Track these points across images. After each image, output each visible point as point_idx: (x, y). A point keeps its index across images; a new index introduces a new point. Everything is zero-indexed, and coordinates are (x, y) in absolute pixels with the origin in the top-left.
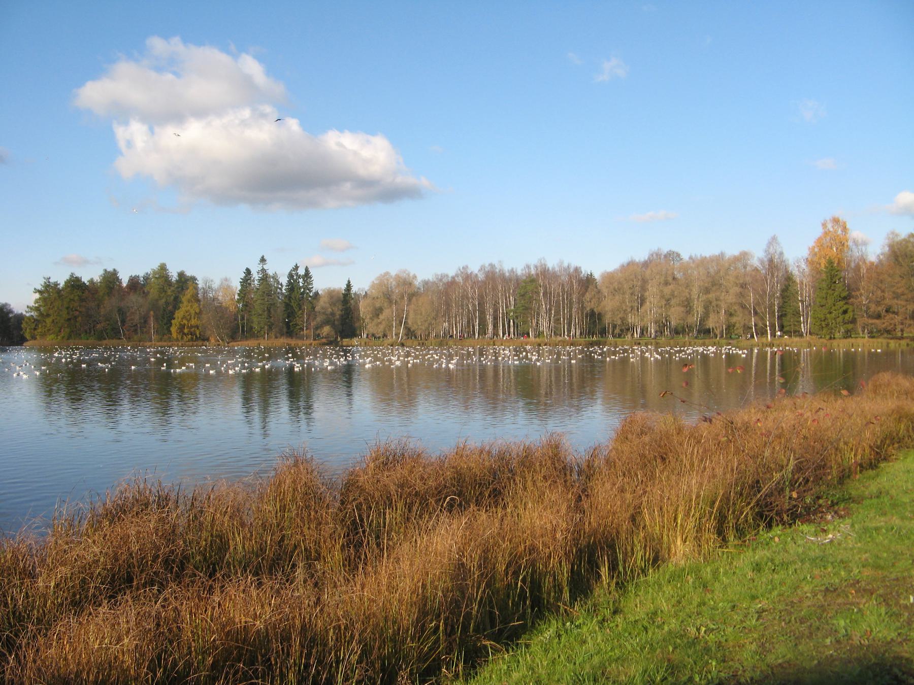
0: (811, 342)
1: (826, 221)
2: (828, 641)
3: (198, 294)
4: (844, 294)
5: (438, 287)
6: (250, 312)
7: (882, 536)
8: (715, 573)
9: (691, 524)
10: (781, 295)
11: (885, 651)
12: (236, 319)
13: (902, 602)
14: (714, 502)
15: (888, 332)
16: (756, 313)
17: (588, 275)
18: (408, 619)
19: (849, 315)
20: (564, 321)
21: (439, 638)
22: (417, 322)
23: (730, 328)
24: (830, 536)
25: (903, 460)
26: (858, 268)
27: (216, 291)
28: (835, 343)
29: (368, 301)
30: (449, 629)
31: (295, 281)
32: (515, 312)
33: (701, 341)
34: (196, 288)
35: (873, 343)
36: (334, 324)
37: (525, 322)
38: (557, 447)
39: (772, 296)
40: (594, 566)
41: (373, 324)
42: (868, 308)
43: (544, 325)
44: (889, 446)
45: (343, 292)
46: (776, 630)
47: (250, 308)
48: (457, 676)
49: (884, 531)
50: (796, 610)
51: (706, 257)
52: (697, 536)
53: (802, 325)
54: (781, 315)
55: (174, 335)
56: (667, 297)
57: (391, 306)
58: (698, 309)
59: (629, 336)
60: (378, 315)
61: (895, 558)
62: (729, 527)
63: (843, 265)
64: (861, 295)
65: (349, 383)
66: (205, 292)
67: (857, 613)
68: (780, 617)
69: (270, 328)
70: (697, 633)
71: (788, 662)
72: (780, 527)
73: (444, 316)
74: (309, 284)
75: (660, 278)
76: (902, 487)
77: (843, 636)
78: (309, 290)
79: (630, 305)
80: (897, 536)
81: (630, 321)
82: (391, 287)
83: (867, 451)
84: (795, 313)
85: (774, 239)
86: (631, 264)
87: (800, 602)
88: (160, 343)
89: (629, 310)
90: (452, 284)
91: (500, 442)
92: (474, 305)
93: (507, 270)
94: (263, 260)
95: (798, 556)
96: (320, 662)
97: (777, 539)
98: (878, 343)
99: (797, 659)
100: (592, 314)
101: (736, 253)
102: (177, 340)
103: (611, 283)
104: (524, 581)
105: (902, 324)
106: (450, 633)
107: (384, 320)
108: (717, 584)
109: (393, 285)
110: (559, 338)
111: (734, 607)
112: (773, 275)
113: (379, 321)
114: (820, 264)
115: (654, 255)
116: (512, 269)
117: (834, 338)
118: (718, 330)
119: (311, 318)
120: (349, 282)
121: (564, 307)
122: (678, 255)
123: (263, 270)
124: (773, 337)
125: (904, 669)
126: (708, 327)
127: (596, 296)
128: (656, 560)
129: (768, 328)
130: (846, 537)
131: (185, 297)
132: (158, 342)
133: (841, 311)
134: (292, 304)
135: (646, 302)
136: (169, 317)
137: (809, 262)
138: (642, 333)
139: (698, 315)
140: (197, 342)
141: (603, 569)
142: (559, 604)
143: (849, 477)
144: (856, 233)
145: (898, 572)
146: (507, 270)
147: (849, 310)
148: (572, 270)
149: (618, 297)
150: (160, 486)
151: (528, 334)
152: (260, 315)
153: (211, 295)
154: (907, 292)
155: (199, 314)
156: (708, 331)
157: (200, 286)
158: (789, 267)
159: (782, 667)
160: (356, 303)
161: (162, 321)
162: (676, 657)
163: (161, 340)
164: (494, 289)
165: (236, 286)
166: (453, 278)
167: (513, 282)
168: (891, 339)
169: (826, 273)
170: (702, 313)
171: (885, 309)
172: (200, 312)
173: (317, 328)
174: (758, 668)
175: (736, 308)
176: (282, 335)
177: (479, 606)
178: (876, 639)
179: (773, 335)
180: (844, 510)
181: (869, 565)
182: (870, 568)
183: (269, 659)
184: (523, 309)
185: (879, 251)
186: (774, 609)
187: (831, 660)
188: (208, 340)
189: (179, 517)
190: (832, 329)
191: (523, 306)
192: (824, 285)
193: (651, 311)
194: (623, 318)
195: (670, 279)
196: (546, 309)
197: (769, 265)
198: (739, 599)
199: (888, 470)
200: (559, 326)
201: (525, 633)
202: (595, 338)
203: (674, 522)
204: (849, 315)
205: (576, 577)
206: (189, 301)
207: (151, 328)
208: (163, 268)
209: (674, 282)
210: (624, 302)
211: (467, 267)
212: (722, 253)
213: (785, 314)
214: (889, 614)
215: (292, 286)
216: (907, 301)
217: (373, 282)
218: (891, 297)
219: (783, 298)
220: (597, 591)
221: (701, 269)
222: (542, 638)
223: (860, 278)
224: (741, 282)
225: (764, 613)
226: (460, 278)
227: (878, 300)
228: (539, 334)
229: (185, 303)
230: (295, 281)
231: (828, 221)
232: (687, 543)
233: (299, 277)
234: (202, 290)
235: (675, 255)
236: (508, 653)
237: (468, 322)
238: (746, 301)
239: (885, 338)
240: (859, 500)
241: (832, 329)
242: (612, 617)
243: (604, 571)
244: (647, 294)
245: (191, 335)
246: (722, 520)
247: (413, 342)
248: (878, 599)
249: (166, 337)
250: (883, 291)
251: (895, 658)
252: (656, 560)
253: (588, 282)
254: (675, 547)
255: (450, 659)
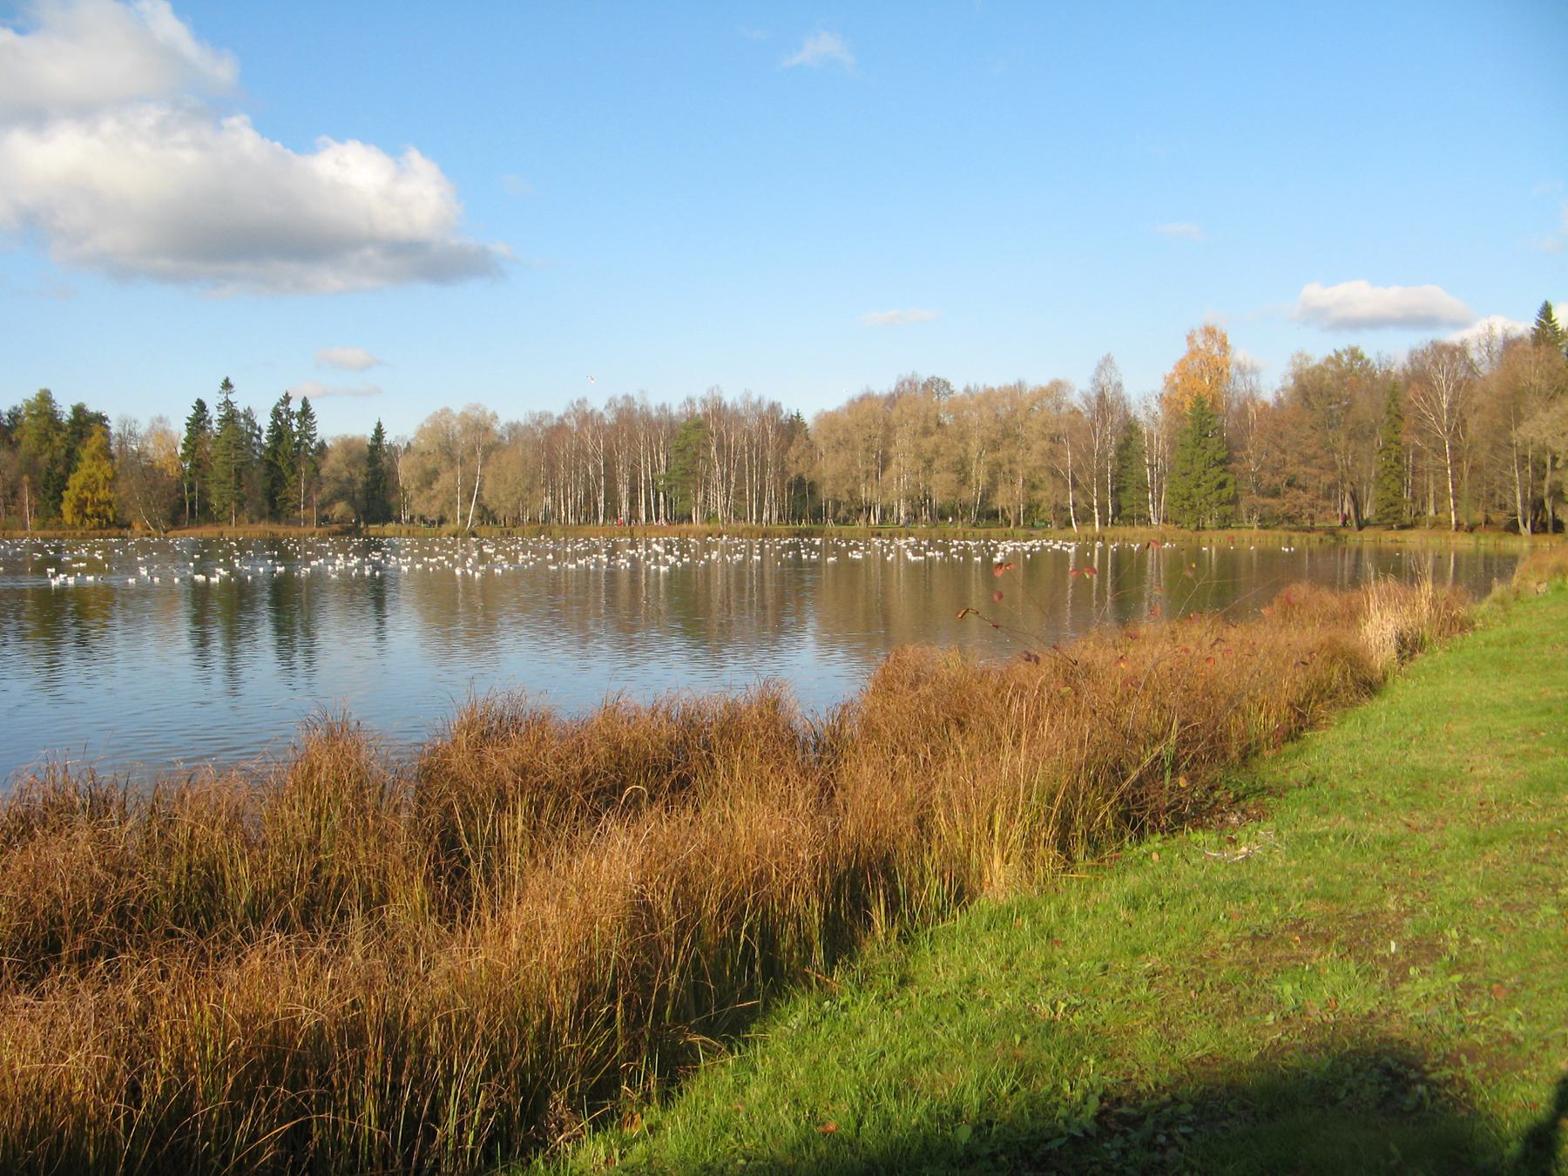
0: (1166, 534)
1: (1193, 331)
2: (1270, 1018)
3: (110, 444)
4: (1221, 455)
5: (534, 435)
6: (203, 477)
7: (1330, 846)
8: (1063, 912)
9: (1017, 833)
10: (1118, 455)
11: (1364, 1032)
12: (180, 490)
13: (1378, 952)
14: (1053, 796)
15: (1290, 519)
16: (1075, 485)
17: (792, 416)
18: (562, 1001)
19: (1229, 491)
20: (751, 494)
21: (615, 1033)
22: (499, 497)
23: (1031, 509)
24: (1244, 849)
25: (1338, 727)
26: (1243, 411)
27: (142, 440)
28: (1205, 536)
29: (412, 459)
30: (633, 1016)
31: (285, 422)
32: (667, 479)
33: (983, 532)
34: (106, 435)
35: (1267, 536)
36: (353, 498)
37: (685, 497)
38: (775, 704)
39: (1103, 456)
40: (860, 907)
41: (422, 498)
42: (1259, 479)
43: (718, 501)
44: (1316, 702)
45: (369, 443)
46: (1183, 1005)
47: (204, 470)
48: (647, 1098)
49: (1331, 838)
50: (1210, 971)
51: (993, 389)
52: (1025, 854)
53: (1151, 506)
54: (1118, 489)
55: (68, 518)
56: (928, 455)
57: (452, 468)
58: (979, 475)
59: (862, 521)
60: (431, 483)
61: (1354, 883)
62: (1077, 838)
63: (1220, 406)
64: (1248, 457)
65: (379, 603)
66: (123, 442)
67: (1310, 971)
68: (1186, 982)
69: (241, 504)
70: (1052, 1013)
71: (1210, 1055)
72: (1159, 836)
73: (545, 485)
74: (310, 428)
75: (915, 424)
76: (1347, 768)
77: (1294, 1010)
78: (309, 438)
79: (864, 469)
80: (1353, 847)
81: (863, 495)
82: (453, 435)
83: (1285, 712)
84: (1140, 485)
85: (1108, 360)
86: (866, 398)
87: (1214, 957)
88: (41, 533)
89: (862, 477)
90: (559, 429)
91: (686, 694)
92: (596, 467)
93: (654, 407)
94: (227, 385)
95: (1200, 883)
96: (417, 1081)
97: (1155, 856)
98: (1274, 537)
99: (1225, 1050)
100: (800, 482)
101: (1044, 382)
102: (73, 526)
103: (832, 431)
104: (750, 931)
105: (1312, 506)
106: (633, 1023)
107: (439, 491)
108: (1068, 933)
109: (456, 431)
110: (742, 525)
111: (1105, 968)
112: (1104, 423)
113: (432, 493)
114: (1183, 404)
115: (906, 385)
116: (664, 405)
117: (1204, 528)
118: (1013, 513)
119: (313, 488)
120: (379, 425)
121: (751, 471)
122: (947, 385)
123: (228, 403)
124: (1103, 526)
125: (1398, 1057)
126: (994, 507)
127: (807, 454)
128: (962, 895)
129: (1096, 510)
130: (1270, 852)
131: (86, 451)
132: (38, 530)
133: (1215, 484)
134: (280, 463)
135: (891, 464)
136: (59, 485)
137: (1165, 400)
138: (883, 518)
139: (977, 487)
140: (109, 531)
141: (875, 910)
142: (807, 970)
143: (1256, 754)
144: (1241, 353)
145: (1362, 905)
146: (654, 407)
147: (1229, 483)
148: (765, 408)
149: (844, 455)
150: (93, 779)
151: (690, 517)
152: (224, 482)
153: (134, 447)
154: (1320, 453)
155: (112, 482)
156: (995, 515)
157: (113, 431)
158: (1130, 408)
159: (1203, 1064)
160: (393, 463)
161: (44, 492)
162: (1029, 1053)
163: (43, 526)
164: (632, 438)
165: (179, 430)
166: (561, 419)
167: (664, 428)
168: (1295, 530)
169: (1192, 419)
170: (985, 484)
171: (1286, 481)
172: (115, 478)
173: (323, 506)
174: (1164, 1066)
175: (1042, 476)
176: (262, 517)
177: (681, 975)
178: (1346, 1012)
179: (1103, 522)
180: (1255, 807)
181: (1317, 896)
182: (1318, 900)
183: (329, 1078)
184: (683, 474)
185: (1278, 385)
186: (1173, 970)
187: (1279, 1049)
188: (129, 526)
189: (128, 836)
190: (1200, 513)
191: (681, 469)
192: (1189, 439)
193: (899, 479)
194: (853, 490)
195: (933, 425)
196: (722, 473)
197: (1099, 405)
198: (1111, 956)
199: (1317, 742)
200: (742, 503)
201: (754, 1021)
202: (804, 525)
203: (989, 829)
204: (1229, 491)
205: (830, 924)
206: (94, 457)
207: (23, 504)
208: (45, 397)
209: (939, 431)
210: (854, 463)
211: (585, 400)
212: (1020, 383)
213: (1125, 488)
214: (1361, 972)
215: (279, 432)
216: (1321, 468)
217: (422, 425)
218: (1296, 461)
219: (1120, 460)
220: (868, 948)
221: (984, 409)
222: (784, 1028)
223: (1247, 429)
224: (1052, 432)
225: (1157, 978)
226: (573, 419)
227: (1276, 465)
228: (710, 517)
229: (87, 462)
230: (285, 422)
231: (1198, 333)
232: (1011, 864)
233: (291, 415)
234: (117, 438)
235: (941, 384)
236: (733, 1055)
237: (587, 496)
238: (1060, 464)
239: (1285, 529)
240: (1278, 791)
241: (1200, 513)
242: (898, 991)
243: (878, 914)
244: (892, 450)
245: (99, 517)
246: (1065, 824)
247: (491, 531)
248: (1340, 949)
249: (52, 521)
250: (1284, 452)
251: (1383, 1041)
252: (960, 895)
253: (792, 429)
254: (990, 871)
255: (635, 1067)
